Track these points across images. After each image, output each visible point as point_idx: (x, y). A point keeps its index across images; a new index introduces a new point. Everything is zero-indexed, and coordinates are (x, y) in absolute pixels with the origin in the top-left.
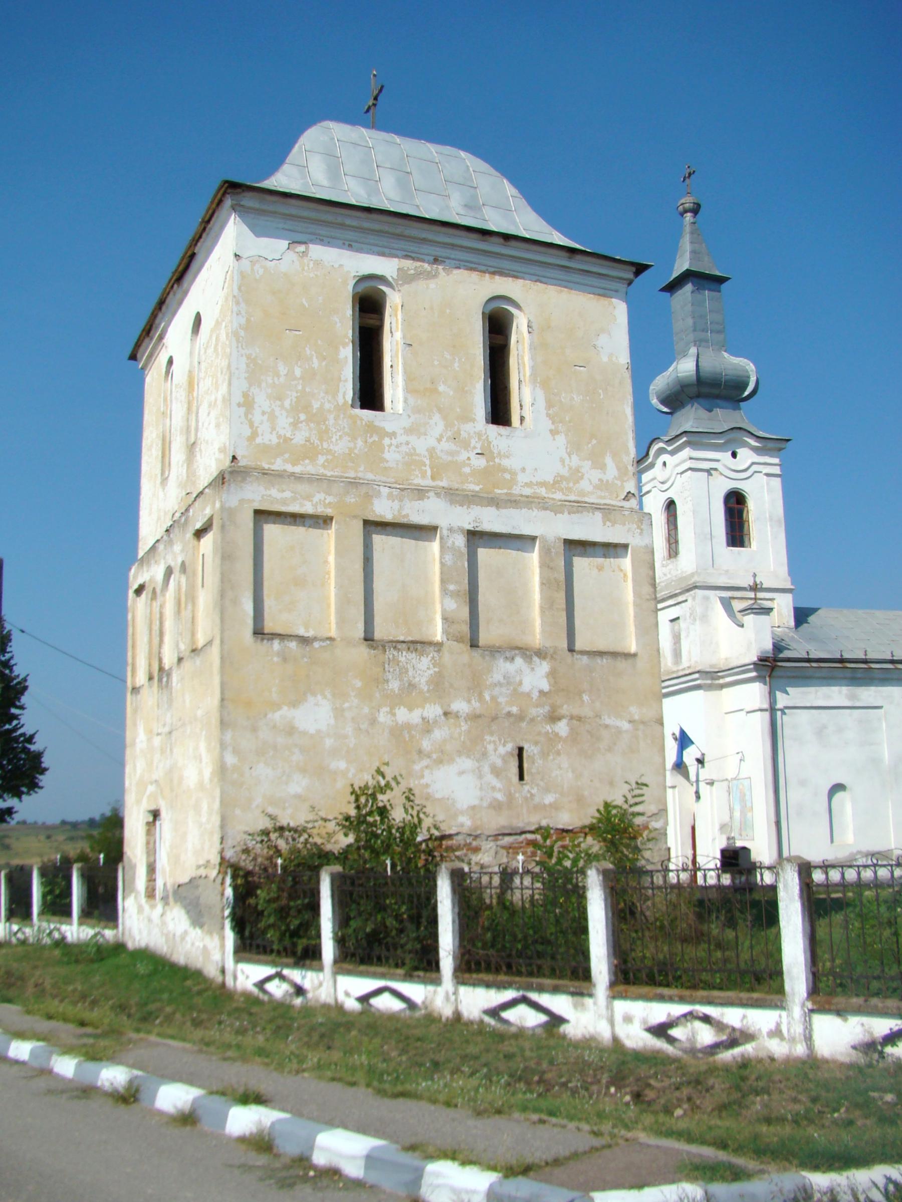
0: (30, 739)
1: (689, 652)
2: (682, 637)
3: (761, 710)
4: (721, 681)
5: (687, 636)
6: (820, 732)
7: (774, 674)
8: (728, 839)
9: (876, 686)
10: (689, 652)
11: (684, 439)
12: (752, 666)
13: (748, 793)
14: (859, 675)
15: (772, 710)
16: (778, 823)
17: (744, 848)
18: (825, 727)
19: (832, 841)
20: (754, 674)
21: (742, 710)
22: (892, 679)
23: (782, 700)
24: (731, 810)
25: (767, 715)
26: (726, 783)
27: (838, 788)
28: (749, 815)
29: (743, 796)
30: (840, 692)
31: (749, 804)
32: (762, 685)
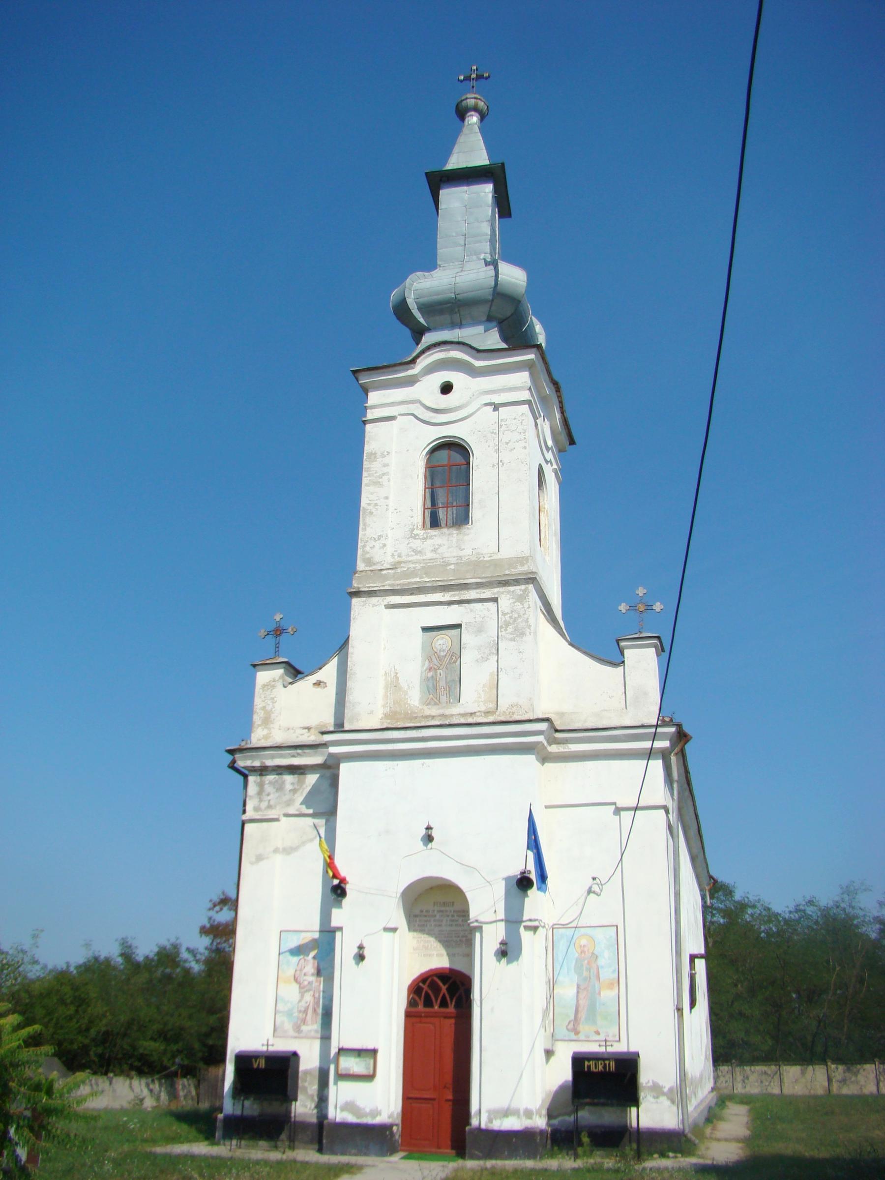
0: (127, 956)
31: (607, 974)
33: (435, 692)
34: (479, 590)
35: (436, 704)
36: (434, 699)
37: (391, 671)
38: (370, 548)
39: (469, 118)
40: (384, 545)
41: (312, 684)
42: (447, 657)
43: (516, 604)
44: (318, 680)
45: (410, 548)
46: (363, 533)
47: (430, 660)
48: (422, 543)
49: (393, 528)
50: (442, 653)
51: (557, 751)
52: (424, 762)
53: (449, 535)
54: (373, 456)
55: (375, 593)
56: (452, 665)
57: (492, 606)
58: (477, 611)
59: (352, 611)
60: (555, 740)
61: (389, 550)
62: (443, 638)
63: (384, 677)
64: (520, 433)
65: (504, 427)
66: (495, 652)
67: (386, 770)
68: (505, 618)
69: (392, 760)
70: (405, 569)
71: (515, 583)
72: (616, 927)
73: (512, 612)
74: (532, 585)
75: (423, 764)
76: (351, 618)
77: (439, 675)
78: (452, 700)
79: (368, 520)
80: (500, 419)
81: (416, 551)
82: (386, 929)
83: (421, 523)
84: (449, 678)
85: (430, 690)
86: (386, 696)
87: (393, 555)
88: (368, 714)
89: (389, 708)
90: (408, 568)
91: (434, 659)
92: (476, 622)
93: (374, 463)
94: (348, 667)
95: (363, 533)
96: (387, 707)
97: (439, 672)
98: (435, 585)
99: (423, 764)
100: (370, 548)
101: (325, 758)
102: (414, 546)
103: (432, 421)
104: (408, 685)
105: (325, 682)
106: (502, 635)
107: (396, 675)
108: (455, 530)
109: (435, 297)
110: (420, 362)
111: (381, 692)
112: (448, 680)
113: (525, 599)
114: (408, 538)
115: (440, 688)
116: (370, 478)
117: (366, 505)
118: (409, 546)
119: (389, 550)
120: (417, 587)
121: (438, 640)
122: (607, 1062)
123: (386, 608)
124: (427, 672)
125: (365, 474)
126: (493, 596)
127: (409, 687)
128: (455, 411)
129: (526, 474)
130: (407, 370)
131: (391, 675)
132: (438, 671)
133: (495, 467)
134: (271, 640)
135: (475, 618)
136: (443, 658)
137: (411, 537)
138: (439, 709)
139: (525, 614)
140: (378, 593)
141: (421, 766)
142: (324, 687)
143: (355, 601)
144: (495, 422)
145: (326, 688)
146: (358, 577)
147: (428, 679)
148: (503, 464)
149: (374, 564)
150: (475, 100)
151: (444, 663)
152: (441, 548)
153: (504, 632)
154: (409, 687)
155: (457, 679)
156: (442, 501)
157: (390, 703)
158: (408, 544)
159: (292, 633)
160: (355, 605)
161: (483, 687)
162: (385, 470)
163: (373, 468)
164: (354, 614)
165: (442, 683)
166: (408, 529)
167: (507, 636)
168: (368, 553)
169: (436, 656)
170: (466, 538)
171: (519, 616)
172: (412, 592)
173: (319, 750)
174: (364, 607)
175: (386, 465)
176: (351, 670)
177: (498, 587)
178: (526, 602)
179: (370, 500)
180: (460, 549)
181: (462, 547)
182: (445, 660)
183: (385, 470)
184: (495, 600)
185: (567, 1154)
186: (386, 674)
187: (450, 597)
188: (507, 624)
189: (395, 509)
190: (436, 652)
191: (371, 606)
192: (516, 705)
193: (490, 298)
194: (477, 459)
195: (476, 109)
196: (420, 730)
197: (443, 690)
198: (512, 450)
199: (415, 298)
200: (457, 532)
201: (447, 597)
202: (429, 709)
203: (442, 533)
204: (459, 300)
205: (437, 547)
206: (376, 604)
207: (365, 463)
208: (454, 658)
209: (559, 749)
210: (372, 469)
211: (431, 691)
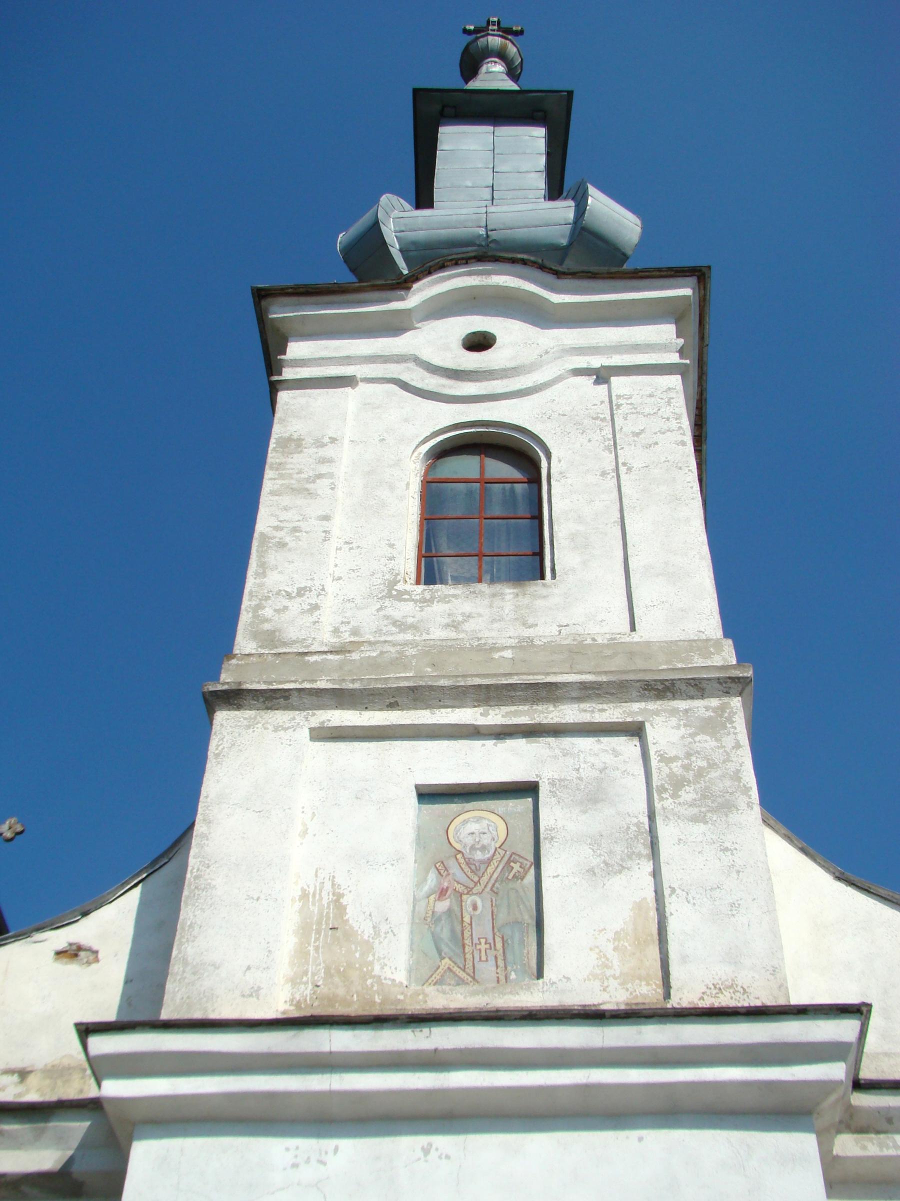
11: (684, 291)
33: (459, 951)
34: (588, 705)
35: (461, 982)
36: (455, 969)
37: (321, 890)
38: (275, 611)
39: (489, 65)
40: (315, 607)
41: (53, 953)
42: (495, 863)
43: (698, 738)
44: (71, 944)
45: (387, 617)
46: (258, 581)
47: (442, 869)
48: (417, 608)
49: (340, 578)
50: (479, 853)
52: (430, 1145)
53: (494, 595)
54: (294, 444)
55: (286, 698)
56: (511, 885)
57: (629, 747)
58: (582, 756)
59: (213, 737)
60: (851, 1116)
61: (328, 618)
62: (481, 818)
63: (298, 905)
64: (668, 419)
65: (625, 409)
66: (647, 851)
67: (295, 1166)
68: (671, 769)
69: (319, 1135)
70: (374, 654)
71: (692, 691)
73: (688, 755)
74: (740, 698)
75: (426, 1151)
76: (210, 754)
77: (470, 909)
78: (513, 976)
79: (272, 557)
80: (614, 395)
81: (403, 624)
83: (413, 576)
84: (502, 917)
85: (443, 947)
86: (301, 953)
87: (336, 631)
88: (243, 996)
89: (310, 986)
90: (382, 653)
91: (454, 869)
92: (580, 779)
93: (295, 456)
94: (189, 869)
95: (258, 581)
96: (307, 983)
97: (469, 902)
98: (462, 684)
99: (426, 1151)
100: (275, 611)
101: (70, 1153)
102: (397, 615)
103: (444, 393)
104: (374, 927)
105: (95, 948)
106: (664, 809)
107: (337, 901)
108: (509, 588)
109: (443, 232)
110: (420, 290)
111: (288, 943)
112: (500, 921)
113: (725, 727)
114: (381, 598)
115: (476, 941)
116: (283, 482)
117: (269, 529)
118: (382, 613)
119: (328, 618)
120: (409, 687)
121: (465, 822)
123: (313, 739)
124: (432, 898)
125: (269, 474)
126: (629, 719)
127: (377, 933)
128: (502, 378)
129: (692, 487)
130: (389, 301)
131: (321, 898)
132: (468, 900)
133: (609, 477)
135: (578, 770)
136: (483, 867)
137: (389, 596)
138: (474, 993)
139: (727, 760)
140: (294, 700)
141: (420, 1154)
142: (89, 963)
143: (222, 717)
144: (602, 402)
145: (94, 966)
146: (237, 665)
147: (436, 919)
148: (629, 469)
149: (285, 644)
150: (503, 40)
151: (485, 879)
152: (471, 620)
153: (671, 800)
154: (377, 933)
155: (529, 919)
156: (455, 574)
157: (314, 974)
158: (378, 610)
159: (9, 835)
160: (222, 725)
161: (614, 939)
162: (324, 469)
163: (291, 463)
164: (218, 746)
165: (482, 929)
166: (379, 581)
167: (682, 810)
168: (267, 620)
169: (462, 861)
170: (540, 603)
171: (712, 765)
172: (392, 700)
173: (51, 1124)
174: (251, 730)
175: (323, 461)
176: (197, 877)
177: (642, 698)
178: (729, 734)
179: (281, 521)
180: (524, 624)
181: (531, 621)
182: (490, 870)
183: (324, 469)
184: (636, 730)
186: (304, 895)
187: (503, 716)
188: (678, 784)
189: (347, 543)
190: (460, 852)
191: (271, 728)
192: (731, 986)
193: (564, 242)
194: (560, 461)
195: (502, 55)
196: (426, 1030)
197: (483, 947)
198: (650, 446)
199: (397, 229)
200: (515, 591)
201: (496, 716)
202: (444, 992)
203: (474, 592)
204: (494, 241)
205: (460, 618)
206: (287, 725)
207: (270, 455)
208: (516, 867)
209: (864, 1148)
210: (288, 466)
211: (445, 949)
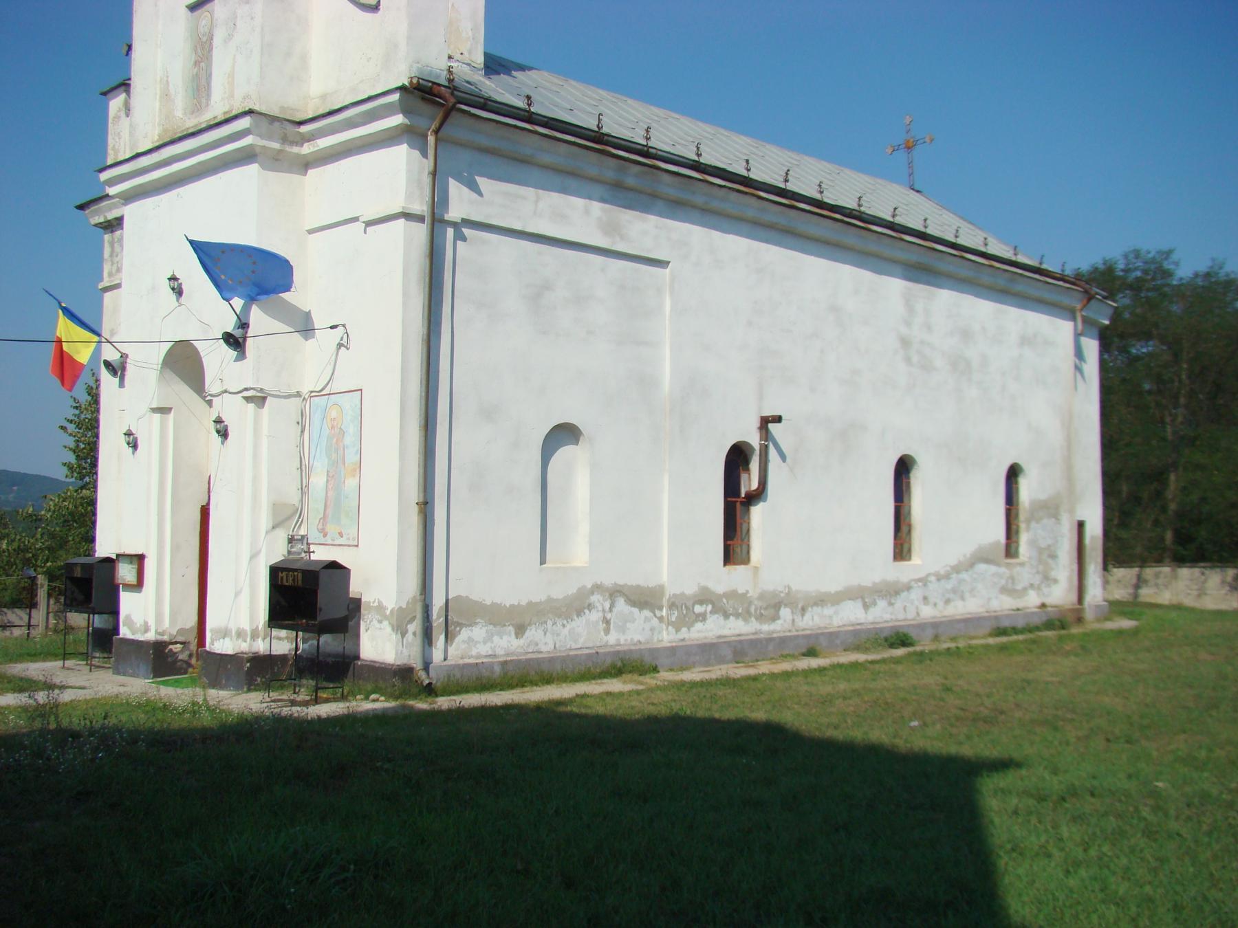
1: (231, 76)
2: (217, 41)
3: (407, 216)
4: (307, 149)
5: (230, 37)
6: (537, 295)
7: (449, 130)
8: (291, 540)
9: (660, 215)
10: (231, 76)
12: (396, 97)
13: (351, 430)
14: (630, 181)
15: (436, 221)
16: (426, 507)
17: (334, 566)
18: (547, 287)
19: (543, 562)
20: (398, 120)
21: (356, 219)
22: (694, 207)
23: (461, 203)
24: (303, 469)
25: (421, 232)
26: (298, 400)
27: (564, 434)
28: (351, 483)
29: (339, 434)
30: (587, 211)
31: (351, 458)
32: (416, 153)
51: (312, 150)
72: (360, 392)
82: (155, 410)
122: (296, 573)
134: (901, 155)
185: (707, 680)
